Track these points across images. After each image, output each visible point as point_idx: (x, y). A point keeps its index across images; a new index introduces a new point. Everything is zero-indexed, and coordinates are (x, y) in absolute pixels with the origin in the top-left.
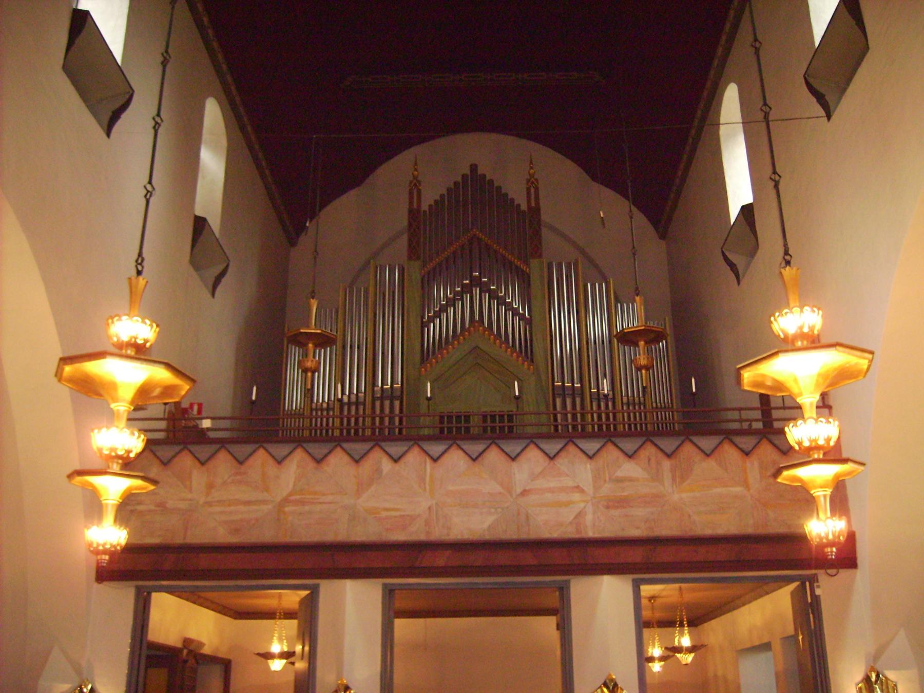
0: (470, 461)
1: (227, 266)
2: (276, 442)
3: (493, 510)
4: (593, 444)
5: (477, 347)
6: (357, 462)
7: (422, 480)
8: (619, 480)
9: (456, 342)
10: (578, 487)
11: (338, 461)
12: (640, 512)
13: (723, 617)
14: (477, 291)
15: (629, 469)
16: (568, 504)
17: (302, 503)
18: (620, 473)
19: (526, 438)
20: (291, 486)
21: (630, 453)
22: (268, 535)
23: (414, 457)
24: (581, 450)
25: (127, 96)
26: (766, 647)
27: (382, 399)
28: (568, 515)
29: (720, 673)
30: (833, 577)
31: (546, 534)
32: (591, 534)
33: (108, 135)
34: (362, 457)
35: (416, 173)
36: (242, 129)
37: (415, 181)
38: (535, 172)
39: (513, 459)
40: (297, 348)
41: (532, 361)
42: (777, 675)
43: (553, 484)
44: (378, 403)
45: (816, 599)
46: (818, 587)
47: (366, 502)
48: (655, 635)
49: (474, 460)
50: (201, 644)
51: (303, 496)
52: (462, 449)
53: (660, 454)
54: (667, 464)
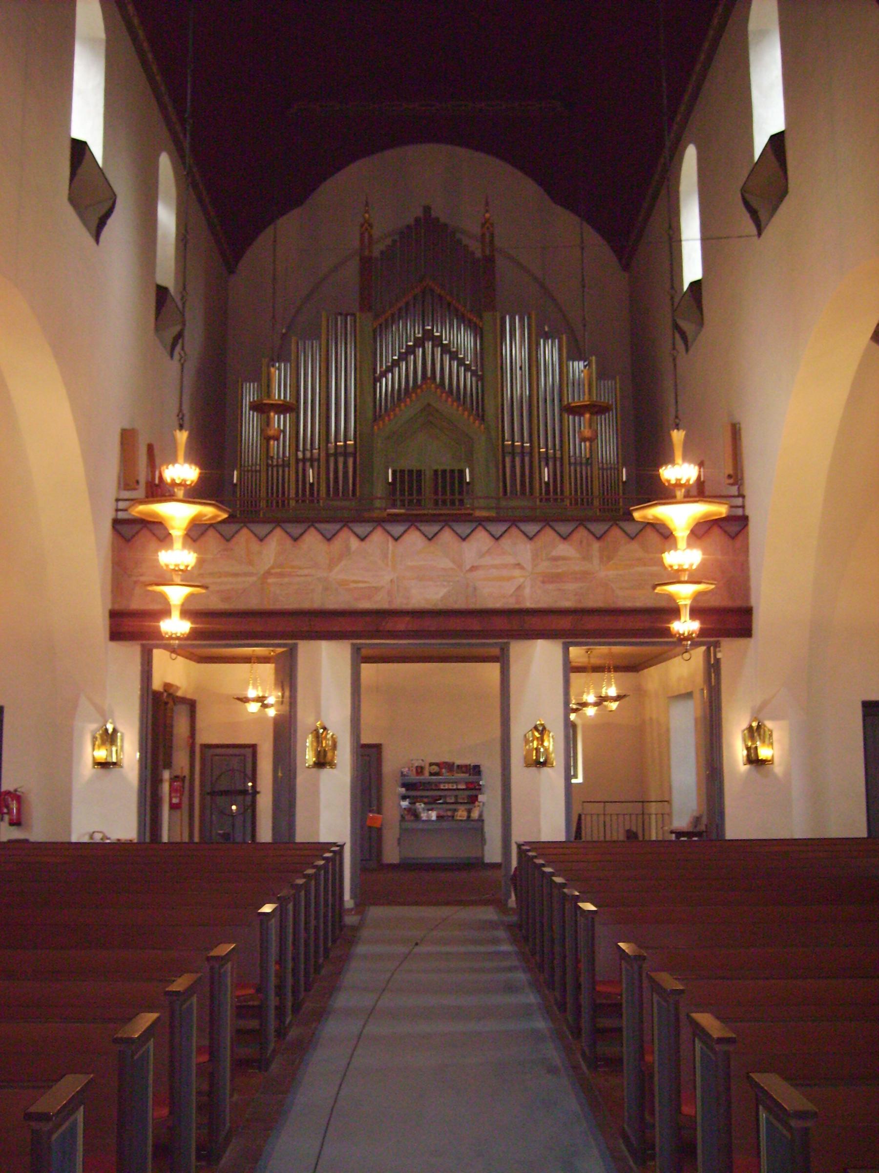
0: (427, 542)
1: (184, 325)
2: (258, 522)
3: (445, 583)
4: (534, 527)
5: (429, 405)
6: (329, 540)
7: (385, 556)
8: (555, 559)
9: (408, 400)
10: (519, 564)
11: (312, 539)
12: (571, 587)
13: (659, 666)
14: (429, 345)
15: (564, 549)
16: (509, 579)
17: (281, 575)
18: (554, 553)
19: (476, 521)
20: (272, 562)
21: (564, 536)
22: (254, 603)
23: (378, 537)
24: (521, 531)
25: (111, 202)
26: (689, 695)
27: (336, 455)
28: (509, 588)
29: (654, 717)
30: (102, 830)
31: (491, 604)
32: (529, 604)
33: (97, 241)
34: (334, 535)
35: (367, 215)
36: (194, 185)
37: (366, 225)
38: (490, 217)
39: (464, 539)
40: (255, 413)
41: (483, 419)
42: (696, 720)
43: (497, 561)
44: (332, 459)
45: (718, 661)
46: (720, 651)
47: (337, 574)
48: (282, 777)
49: (430, 540)
50: (178, 688)
51: (283, 570)
52: (420, 530)
53: (591, 537)
54: (596, 545)
